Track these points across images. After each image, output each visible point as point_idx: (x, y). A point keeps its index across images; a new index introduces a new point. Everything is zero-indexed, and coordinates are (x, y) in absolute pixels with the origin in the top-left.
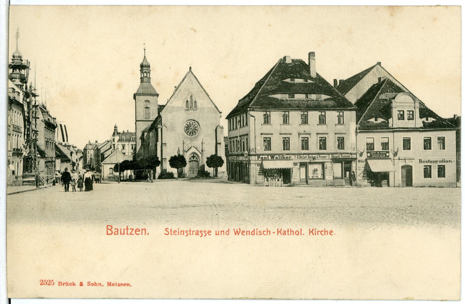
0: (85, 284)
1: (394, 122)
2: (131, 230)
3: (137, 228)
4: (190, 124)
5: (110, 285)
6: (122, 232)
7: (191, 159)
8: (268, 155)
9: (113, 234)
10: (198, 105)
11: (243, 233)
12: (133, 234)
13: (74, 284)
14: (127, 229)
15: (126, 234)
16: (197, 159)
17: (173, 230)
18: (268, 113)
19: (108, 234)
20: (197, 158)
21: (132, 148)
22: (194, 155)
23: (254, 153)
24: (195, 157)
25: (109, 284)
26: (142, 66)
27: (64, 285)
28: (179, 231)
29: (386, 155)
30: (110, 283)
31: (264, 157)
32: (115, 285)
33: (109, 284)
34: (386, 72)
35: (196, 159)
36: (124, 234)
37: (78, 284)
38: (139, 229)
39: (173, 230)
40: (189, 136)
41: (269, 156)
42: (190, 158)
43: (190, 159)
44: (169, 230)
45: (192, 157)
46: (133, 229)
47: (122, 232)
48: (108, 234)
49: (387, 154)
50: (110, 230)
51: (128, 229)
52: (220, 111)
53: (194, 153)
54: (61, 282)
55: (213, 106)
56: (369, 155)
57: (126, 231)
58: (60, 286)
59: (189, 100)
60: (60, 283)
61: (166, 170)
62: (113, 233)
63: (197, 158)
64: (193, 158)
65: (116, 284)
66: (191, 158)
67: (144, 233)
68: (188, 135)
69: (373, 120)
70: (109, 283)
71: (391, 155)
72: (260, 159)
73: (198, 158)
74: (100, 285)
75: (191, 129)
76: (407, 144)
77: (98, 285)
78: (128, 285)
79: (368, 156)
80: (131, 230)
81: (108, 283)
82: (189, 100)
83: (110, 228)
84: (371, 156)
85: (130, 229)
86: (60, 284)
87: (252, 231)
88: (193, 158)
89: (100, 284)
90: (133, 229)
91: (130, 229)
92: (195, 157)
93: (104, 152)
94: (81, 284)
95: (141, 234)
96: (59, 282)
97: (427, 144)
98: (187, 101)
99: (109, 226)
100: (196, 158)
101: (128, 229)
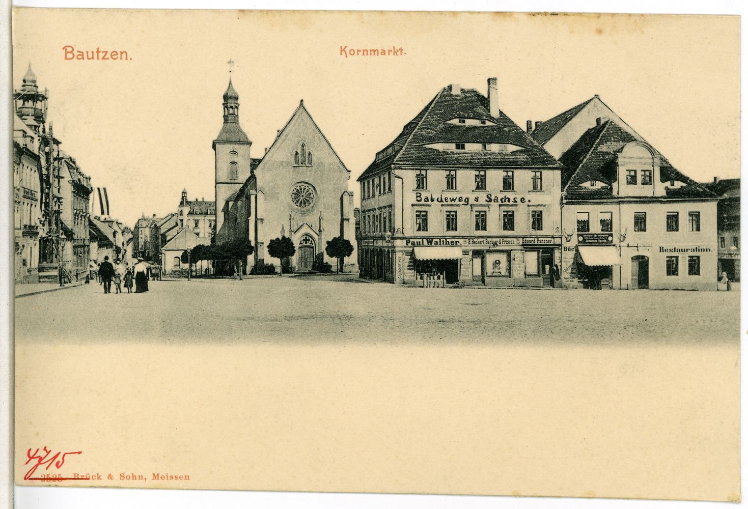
1: (622, 188)
4: (301, 189)
6: (90, 56)
7: (302, 244)
8: (422, 238)
9: (75, 58)
10: (314, 158)
12: (108, 59)
14: (98, 52)
16: (311, 243)
18: (423, 172)
20: (311, 242)
21: (210, 226)
22: (306, 238)
23: (401, 235)
24: (309, 240)
26: (226, 97)
29: (607, 240)
31: (417, 242)
35: (310, 244)
36: (93, 58)
40: (299, 208)
41: (425, 241)
42: (301, 242)
43: (301, 243)
45: (303, 240)
46: (107, 52)
47: (90, 56)
48: (66, 58)
49: (610, 238)
50: (71, 52)
51: (100, 52)
52: (349, 170)
53: (307, 234)
55: (338, 161)
56: (581, 239)
57: (95, 54)
59: (299, 151)
63: (311, 242)
64: (306, 243)
66: (302, 242)
68: (298, 206)
69: (587, 185)
71: (616, 240)
72: (410, 245)
73: (313, 242)
74: (141, 478)
75: (303, 196)
76: (640, 222)
77: (137, 478)
79: (579, 242)
80: (104, 54)
81: (154, 474)
82: (299, 151)
83: (69, 49)
84: (584, 240)
88: (306, 243)
90: (107, 52)
91: (103, 52)
92: (309, 240)
93: (166, 232)
97: (672, 222)
98: (297, 153)
99: (66, 47)
100: (310, 242)
101: (100, 52)
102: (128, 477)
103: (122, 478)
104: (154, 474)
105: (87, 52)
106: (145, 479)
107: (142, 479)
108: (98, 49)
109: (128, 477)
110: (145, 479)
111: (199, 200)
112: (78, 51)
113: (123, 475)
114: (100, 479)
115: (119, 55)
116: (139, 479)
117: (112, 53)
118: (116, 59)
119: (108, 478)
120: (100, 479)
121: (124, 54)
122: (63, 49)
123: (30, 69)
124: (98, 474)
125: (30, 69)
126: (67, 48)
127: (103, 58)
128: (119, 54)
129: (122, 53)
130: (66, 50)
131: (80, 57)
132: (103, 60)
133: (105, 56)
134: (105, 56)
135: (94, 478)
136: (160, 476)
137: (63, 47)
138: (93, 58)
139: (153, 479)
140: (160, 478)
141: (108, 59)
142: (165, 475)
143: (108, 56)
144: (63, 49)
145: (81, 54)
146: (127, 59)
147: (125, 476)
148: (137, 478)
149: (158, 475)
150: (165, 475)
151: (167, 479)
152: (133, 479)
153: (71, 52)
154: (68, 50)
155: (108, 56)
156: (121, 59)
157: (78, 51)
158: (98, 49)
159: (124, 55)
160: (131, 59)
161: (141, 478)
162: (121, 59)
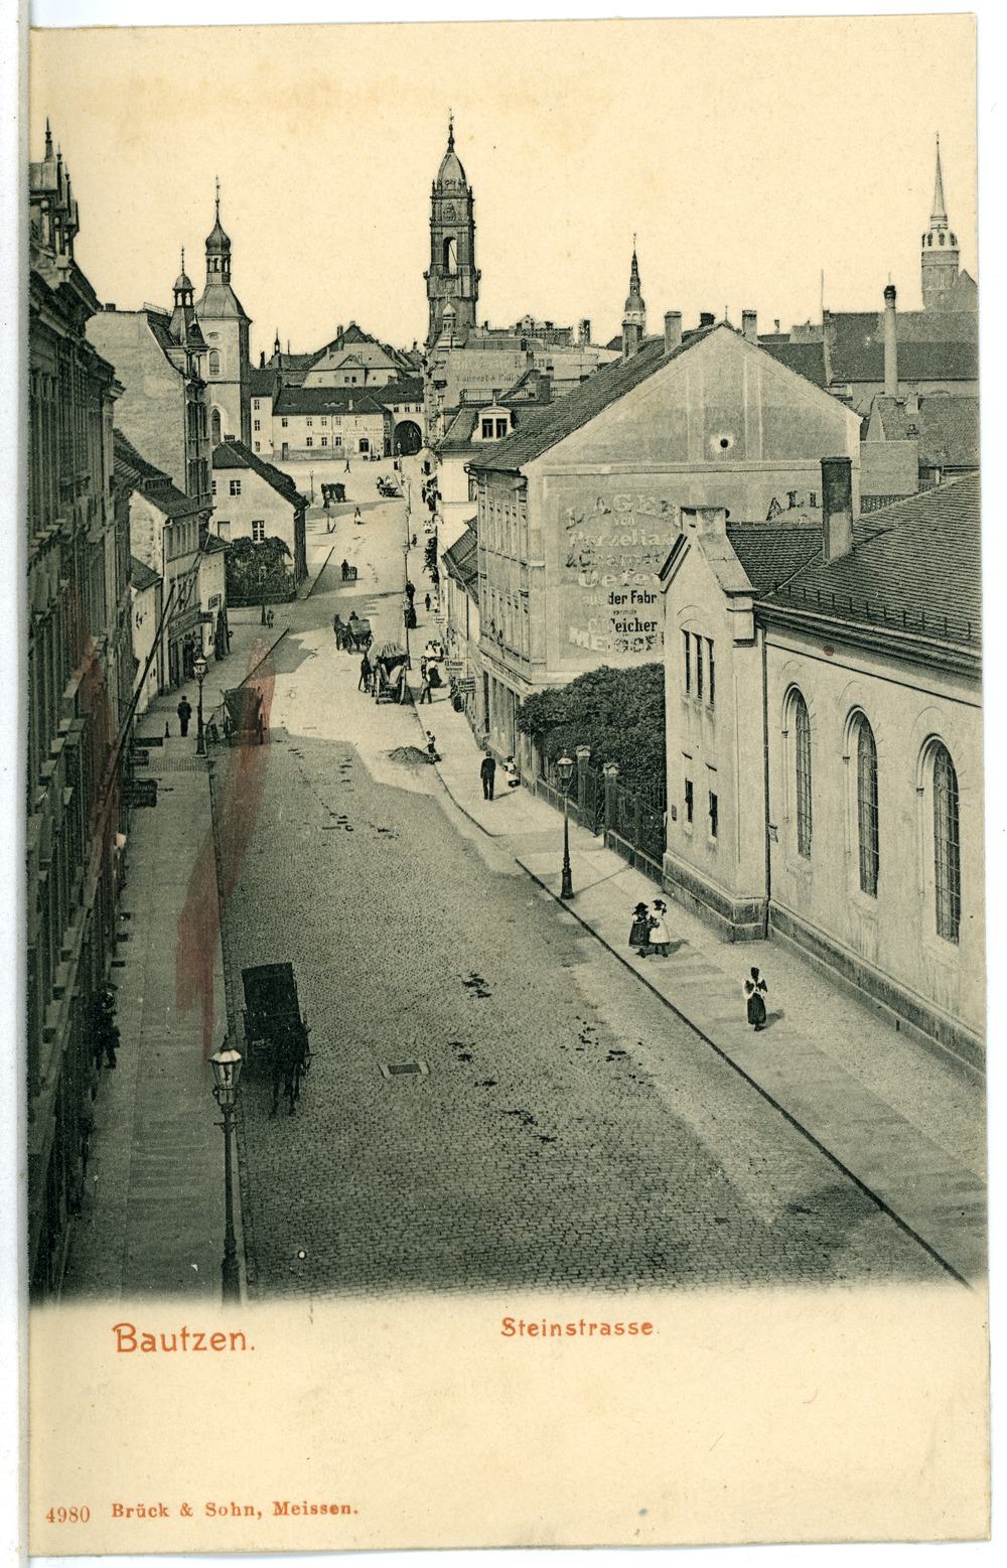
0: (199, 1510)
2: (198, 1338)
3: (218, 1331)
5: (284, 1511)
6: (169, 1344)
9: (139, 1349)
11: (218, 1341)
12: (205, 1349)
13: (163, 1512)
14: (184, 1335)
15: (561, 1325)
17: (527, 1323)
19: (120, 1350)
25: (281, 1509)
27: (128, 1516)
28: (544, 1326)
30: (286, 1504)
32: (302, 1510)
33: (281, 1509)
34: (442, 1545)
36: (174, 1348)
37: (174, 1511)
38: (224, 1333)
39: (587, 1322)
44: (516, 1325)
46: (202, 1336)
47: (169, 1344)
48: (120, 1350)
50: (130, 1337)
51: (188, 1335)
54: (121, 1507)
57: (179, 1340)
58: (118, 1518)
60: (118, 1507)
61: (118, 1046)
62: (139, 1345)
65: (305, 1507)
67: (241, 1346)
70: (281, 1505)
74: (249, 1511)
77: (243, 1512)
78: (346, 1509)
80: (198, 1338)
81: (277, 1504)
83: (126, 1331)
85: (195, 1335)
86: (118, 1513)
87: (137, 1350)
89: (250, 1510)
90: (202, 1336)
91: (195, 1335)
94: (186, 1511)
95: (229, 1346)
96: (115, 1505)
99: (122, 1325)
101: (188, 1335)
102: (223, 1512)
103: (212, 1513)
104: (277, 1504)
105: (163, 1336)
106: (260, 1514)
107: (252, 1514)
108: (184, 1330)
109: (223, 1512)
110: (260, 1514)
111: (292, 446)
112: (144, 1335)
113: (211, 1506)
114: (166, 1515)
115: (228, 1341)
116: (247, 1514)
117: (213, 1337)
118: (221, 1349)
119: (182, 1514)
120: (166, 1515)
121: (239, 1338)
122: (114, 1329)
123: (218, 225)
124: (161, 1505)
125: (218, 225)
126: (121, 1328)
127: (196, 1348)
128: (228, 1339)
129: (233, 1337)
130: (119, 1332)
131: (147, 1346)
132: (196, 1352)
133: (199, 1343)
134: (199, 1343)
135: (153, 1513)
136: (290, 1507)
137: (113, 1326)
138: (174, 1348)
139: (276, 1514)
140: (289, 1511)
141: (205, 1349)
142: (301, 1505)
143: (206, 1342)
144: (114, 1329)
145: (150, 1340)
146: (244, 1348)
147: (217, 1509)
148: (243, 1512)
149: (286, 1504)
150: (301, 1505)
151: (306, 1513)
152: (233, 1514)
153: (130, 1337)
154: (123, 1333)
155: (206, 1342)
156: (233, 1348)
157: (144, 1335)
158: (184, 1330)
159: (238, 1340)
160: (253, 1348)
161: (249, 1511)
162: (233, 1348)
